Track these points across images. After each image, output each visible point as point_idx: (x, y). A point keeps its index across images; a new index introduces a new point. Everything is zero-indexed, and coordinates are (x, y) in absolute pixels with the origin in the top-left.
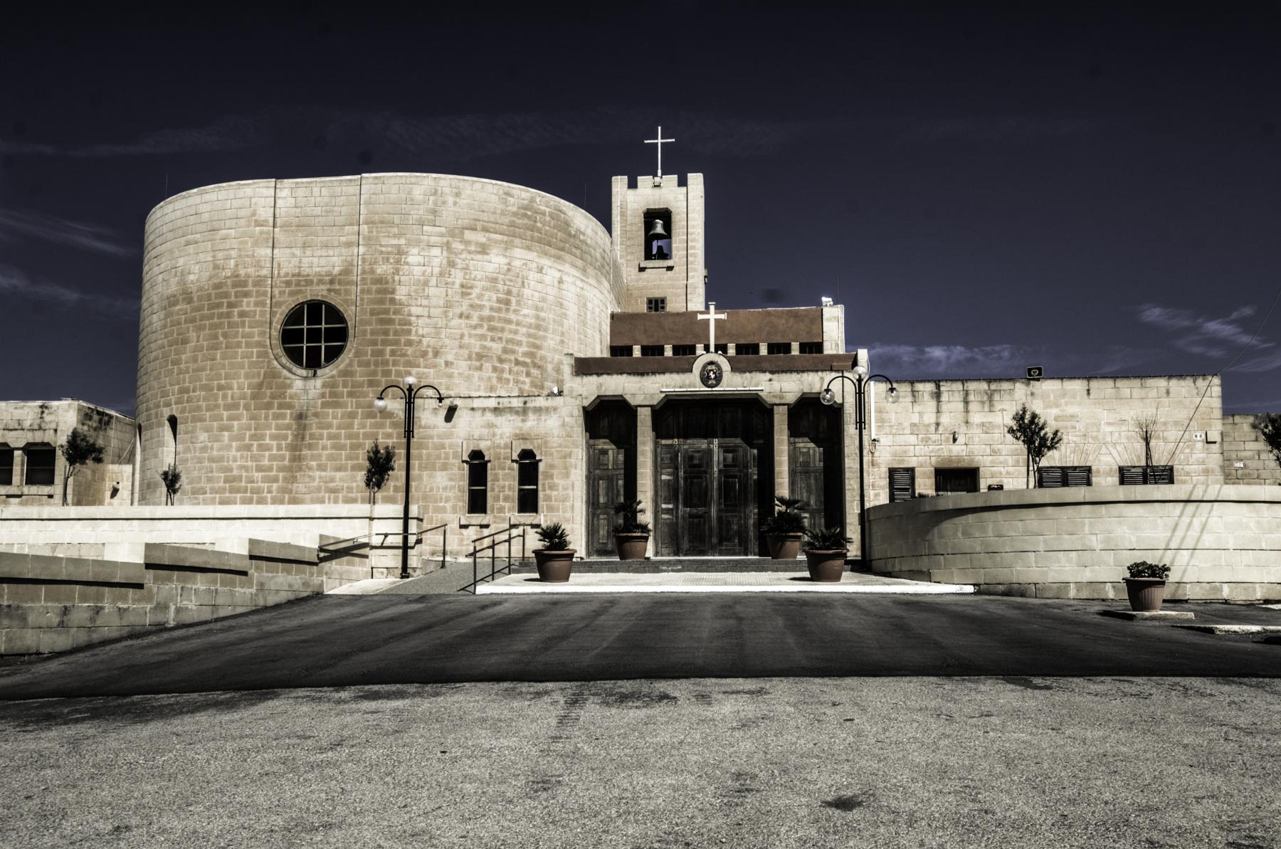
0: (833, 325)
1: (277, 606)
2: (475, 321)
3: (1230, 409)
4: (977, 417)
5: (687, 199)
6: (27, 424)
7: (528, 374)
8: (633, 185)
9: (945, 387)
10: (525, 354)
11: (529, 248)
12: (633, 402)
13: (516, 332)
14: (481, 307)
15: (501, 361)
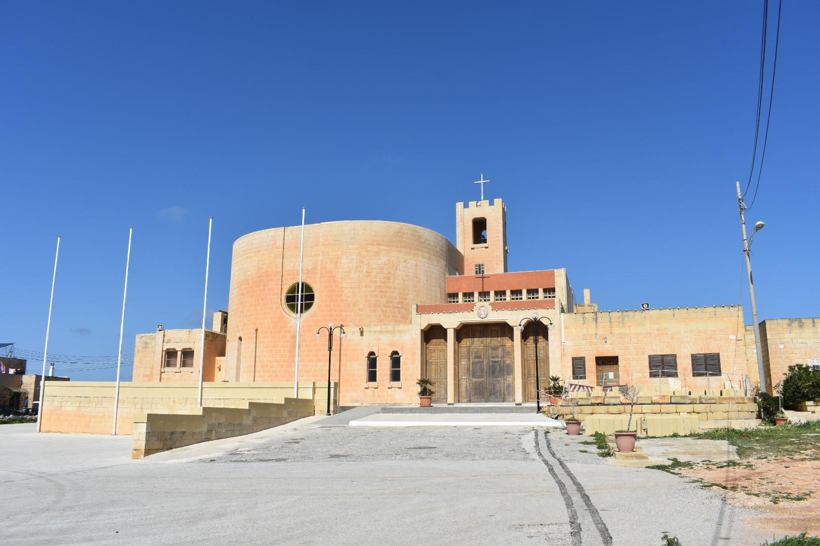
1: (425, 448)
4: (617, 331)
7: (399, 312)
8: (466, 206)
10: (398, 303)
11: (400, 251)
13: (393, 292)
15: (385, 307)
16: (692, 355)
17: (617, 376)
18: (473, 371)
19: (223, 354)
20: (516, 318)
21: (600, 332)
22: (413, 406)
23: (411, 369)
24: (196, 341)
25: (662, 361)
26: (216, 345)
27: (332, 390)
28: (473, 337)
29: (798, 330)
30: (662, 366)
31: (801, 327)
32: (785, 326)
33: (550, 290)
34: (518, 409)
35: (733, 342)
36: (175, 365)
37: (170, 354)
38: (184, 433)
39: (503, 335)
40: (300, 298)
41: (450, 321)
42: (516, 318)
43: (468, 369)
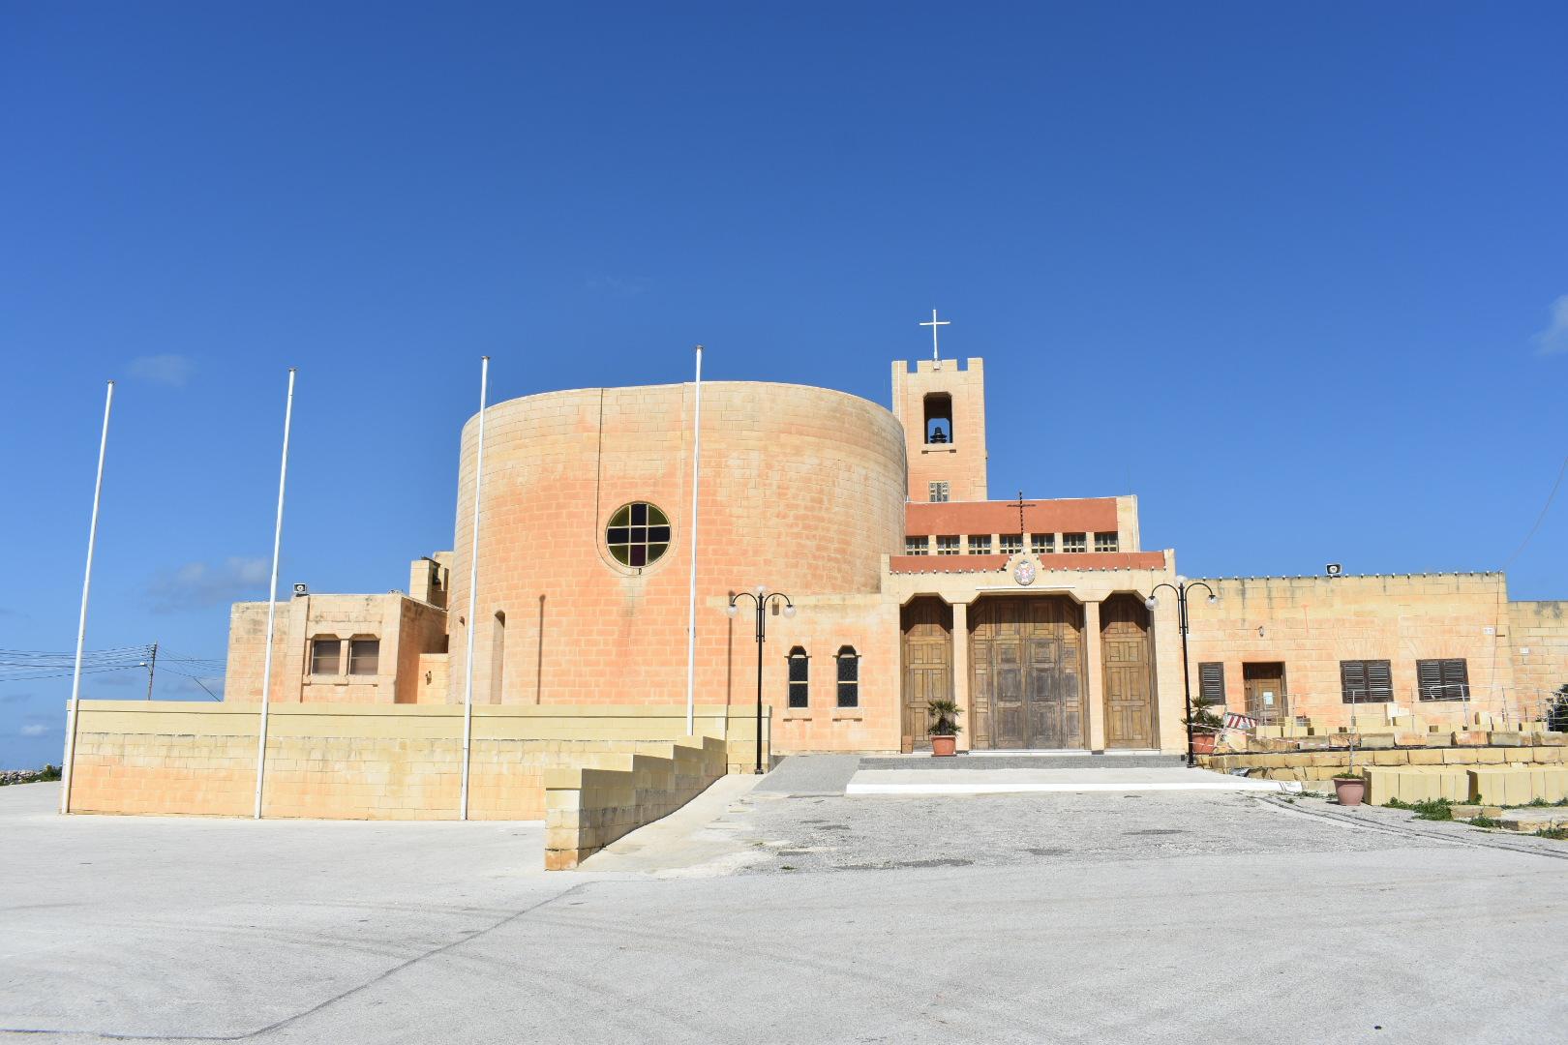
0: (1127, 516)
2: (790, 520)
3: (1514, 597)
4: (1281, 614)
5: (966, 384)
6: (353, 616)
8: (912, 368)
9: (1248, 584)
10: (837, 551)
12: (948, 599)
14: (797, 506)
15: (815, 557)
16: (1419, 663)
17: (1282, 702)
18: (1000, 689)
19: (442, 645)
20: (1091, 587)
21: (1251, 616)
22: (886, 755)
23: (879, 679)
24: (383, 617)
25: (1365, 672)
26: (428, 630)
27: (765, 722)
28: (999, 621)
29: (1552, 623)
30: (1365, 681)
31: (1557, 616)
32: (1530, 615)
33: (1108, 537)
34: (1097, 759)
35: (1490, 639)
36: (335, 670)
37: (323, 647)
38: (615, 810)
39: (1058, 619)
40: (639, 534)
41: (959, 590)
42: (1091, 587)
43: (990, 684)
